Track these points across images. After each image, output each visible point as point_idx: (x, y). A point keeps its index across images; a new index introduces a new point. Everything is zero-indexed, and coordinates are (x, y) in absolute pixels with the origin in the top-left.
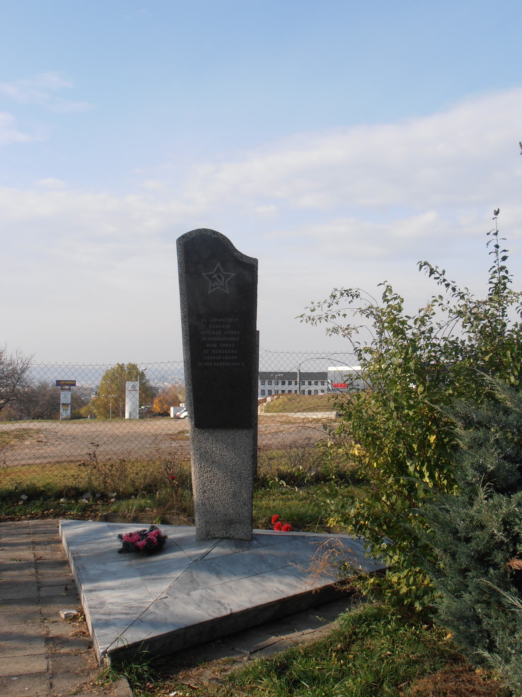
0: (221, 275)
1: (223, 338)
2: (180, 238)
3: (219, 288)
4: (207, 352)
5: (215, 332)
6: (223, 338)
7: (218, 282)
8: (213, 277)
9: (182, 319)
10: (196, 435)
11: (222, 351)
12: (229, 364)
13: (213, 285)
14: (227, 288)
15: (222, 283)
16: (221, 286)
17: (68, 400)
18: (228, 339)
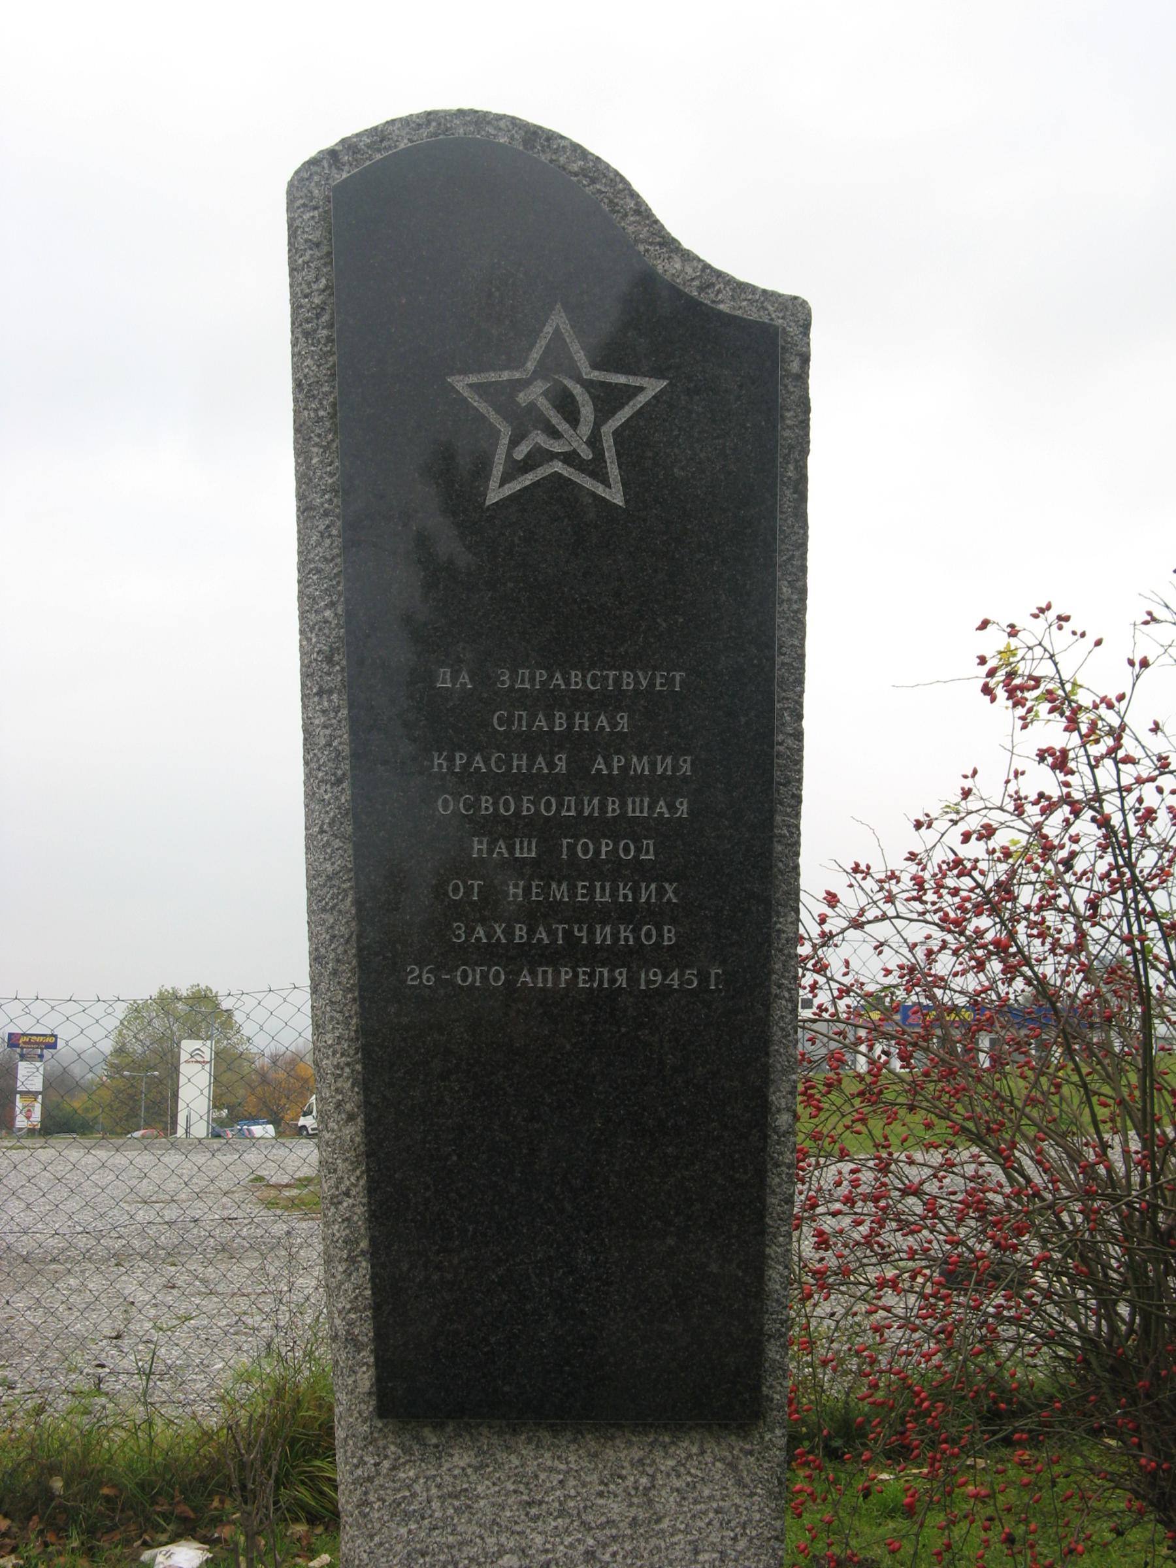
0: (577, 390)
1: (579, 804)
2: (313, 162)
3: (558, 467)
4: (469, 890)
5: (532, 761)
6: (579, 804)
7: (555, 434)
8: (522, 398)
9: (307, 674)
10: (386, 1464)
11: (572, 889)
12: (622, 981)
13: (521, 452)
14: (613, 471)
15: (576, 440)
16: (570, 458)
17: (37, 1084)
18: (613, 808)
